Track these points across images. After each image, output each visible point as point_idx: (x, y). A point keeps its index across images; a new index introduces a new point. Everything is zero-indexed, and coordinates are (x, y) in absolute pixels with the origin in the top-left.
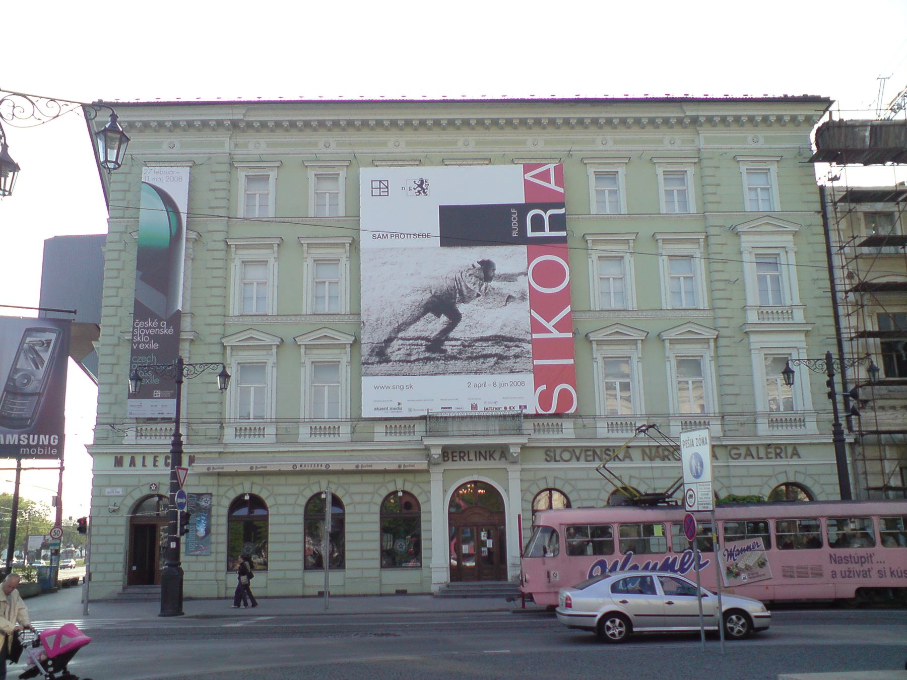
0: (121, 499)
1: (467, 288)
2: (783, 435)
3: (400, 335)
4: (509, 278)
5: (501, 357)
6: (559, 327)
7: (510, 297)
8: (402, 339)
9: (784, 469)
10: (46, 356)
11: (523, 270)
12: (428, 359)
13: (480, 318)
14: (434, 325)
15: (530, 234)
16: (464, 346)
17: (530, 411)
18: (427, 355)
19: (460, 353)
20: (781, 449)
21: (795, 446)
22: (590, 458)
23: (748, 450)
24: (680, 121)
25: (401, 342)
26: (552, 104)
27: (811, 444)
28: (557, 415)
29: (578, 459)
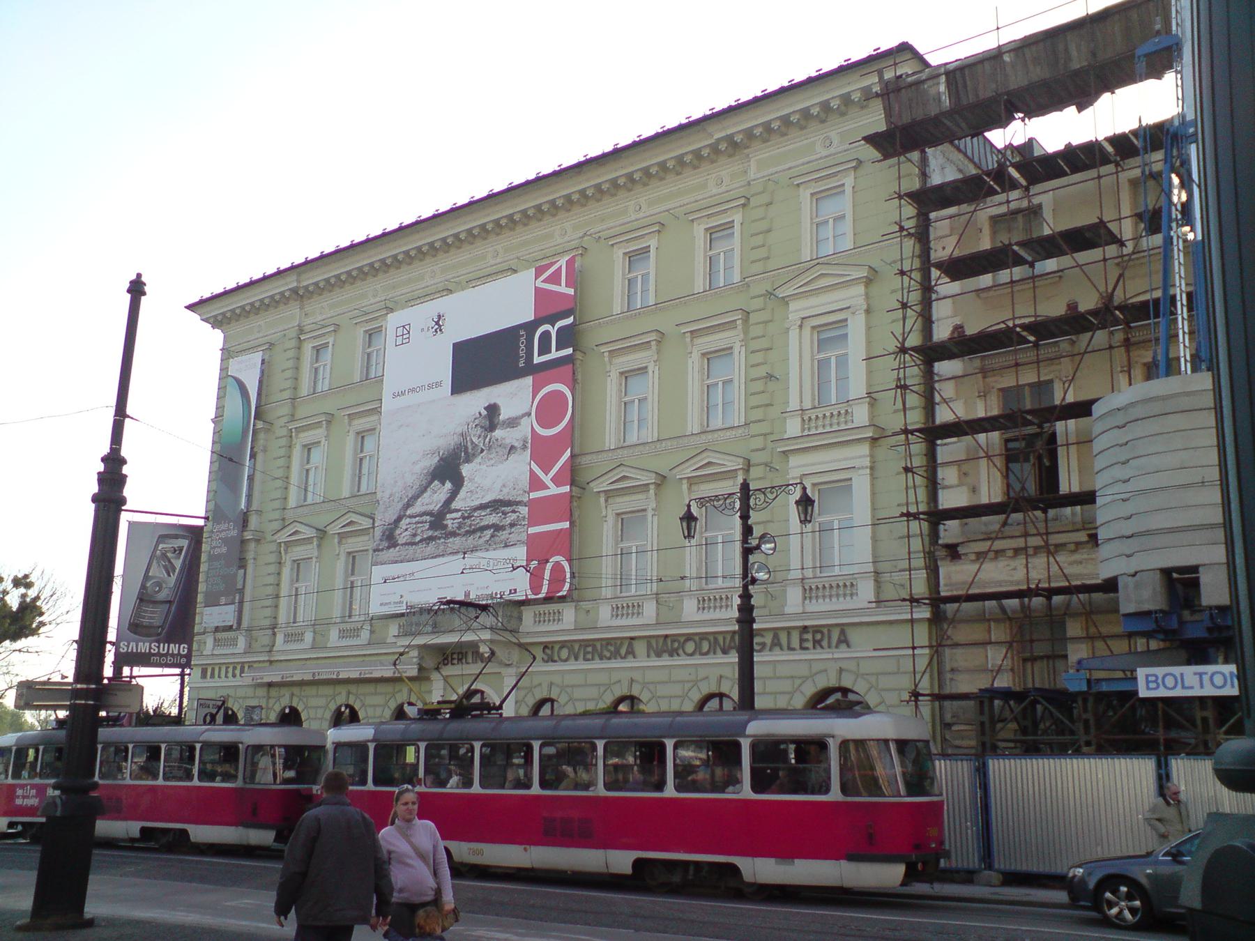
0: (788, 697)
1: (472, 442)
2: (823, 610)
3: (408, 512)
4: (513, 423)
5: (497, 528)
6: (557, 481)
7: (512, 448)
8: (410, 517)
9: (820, 666)
10: (178, 564)
11: (527, 410)
12: (431, 539)
13: (488, 478)
14: (437, 496)
15: (537, 360)
16: (464, 518)
17: (520, 596)
18: (430, 533)
19: (459, 528)
20: (822, 633)
21: (843, 628)
22: (589, 656)
23: (776, 636)
24: (715, 148)
25: (408, 520)
26: (554, 178)
27: (891, 622)
28: (548, 599)
29: (576, 659)
